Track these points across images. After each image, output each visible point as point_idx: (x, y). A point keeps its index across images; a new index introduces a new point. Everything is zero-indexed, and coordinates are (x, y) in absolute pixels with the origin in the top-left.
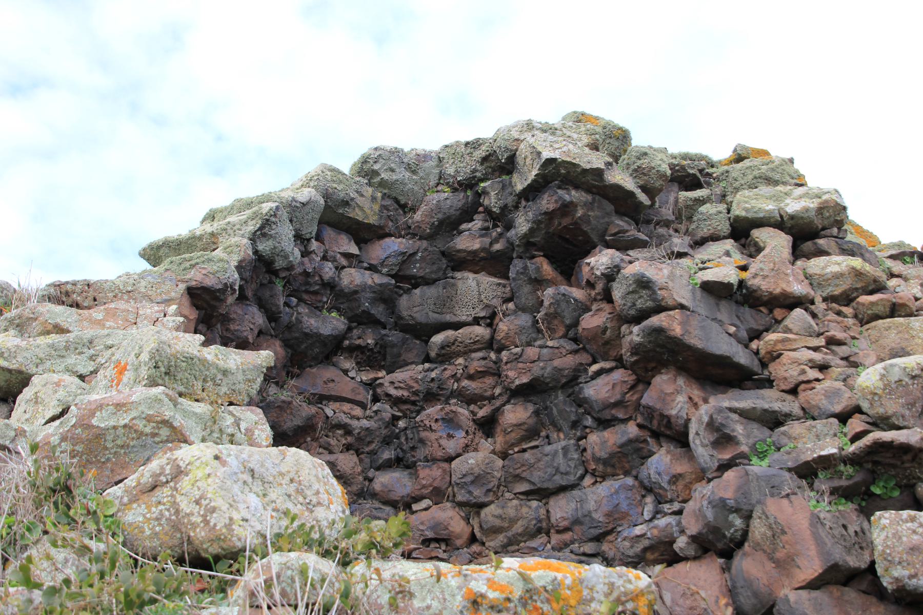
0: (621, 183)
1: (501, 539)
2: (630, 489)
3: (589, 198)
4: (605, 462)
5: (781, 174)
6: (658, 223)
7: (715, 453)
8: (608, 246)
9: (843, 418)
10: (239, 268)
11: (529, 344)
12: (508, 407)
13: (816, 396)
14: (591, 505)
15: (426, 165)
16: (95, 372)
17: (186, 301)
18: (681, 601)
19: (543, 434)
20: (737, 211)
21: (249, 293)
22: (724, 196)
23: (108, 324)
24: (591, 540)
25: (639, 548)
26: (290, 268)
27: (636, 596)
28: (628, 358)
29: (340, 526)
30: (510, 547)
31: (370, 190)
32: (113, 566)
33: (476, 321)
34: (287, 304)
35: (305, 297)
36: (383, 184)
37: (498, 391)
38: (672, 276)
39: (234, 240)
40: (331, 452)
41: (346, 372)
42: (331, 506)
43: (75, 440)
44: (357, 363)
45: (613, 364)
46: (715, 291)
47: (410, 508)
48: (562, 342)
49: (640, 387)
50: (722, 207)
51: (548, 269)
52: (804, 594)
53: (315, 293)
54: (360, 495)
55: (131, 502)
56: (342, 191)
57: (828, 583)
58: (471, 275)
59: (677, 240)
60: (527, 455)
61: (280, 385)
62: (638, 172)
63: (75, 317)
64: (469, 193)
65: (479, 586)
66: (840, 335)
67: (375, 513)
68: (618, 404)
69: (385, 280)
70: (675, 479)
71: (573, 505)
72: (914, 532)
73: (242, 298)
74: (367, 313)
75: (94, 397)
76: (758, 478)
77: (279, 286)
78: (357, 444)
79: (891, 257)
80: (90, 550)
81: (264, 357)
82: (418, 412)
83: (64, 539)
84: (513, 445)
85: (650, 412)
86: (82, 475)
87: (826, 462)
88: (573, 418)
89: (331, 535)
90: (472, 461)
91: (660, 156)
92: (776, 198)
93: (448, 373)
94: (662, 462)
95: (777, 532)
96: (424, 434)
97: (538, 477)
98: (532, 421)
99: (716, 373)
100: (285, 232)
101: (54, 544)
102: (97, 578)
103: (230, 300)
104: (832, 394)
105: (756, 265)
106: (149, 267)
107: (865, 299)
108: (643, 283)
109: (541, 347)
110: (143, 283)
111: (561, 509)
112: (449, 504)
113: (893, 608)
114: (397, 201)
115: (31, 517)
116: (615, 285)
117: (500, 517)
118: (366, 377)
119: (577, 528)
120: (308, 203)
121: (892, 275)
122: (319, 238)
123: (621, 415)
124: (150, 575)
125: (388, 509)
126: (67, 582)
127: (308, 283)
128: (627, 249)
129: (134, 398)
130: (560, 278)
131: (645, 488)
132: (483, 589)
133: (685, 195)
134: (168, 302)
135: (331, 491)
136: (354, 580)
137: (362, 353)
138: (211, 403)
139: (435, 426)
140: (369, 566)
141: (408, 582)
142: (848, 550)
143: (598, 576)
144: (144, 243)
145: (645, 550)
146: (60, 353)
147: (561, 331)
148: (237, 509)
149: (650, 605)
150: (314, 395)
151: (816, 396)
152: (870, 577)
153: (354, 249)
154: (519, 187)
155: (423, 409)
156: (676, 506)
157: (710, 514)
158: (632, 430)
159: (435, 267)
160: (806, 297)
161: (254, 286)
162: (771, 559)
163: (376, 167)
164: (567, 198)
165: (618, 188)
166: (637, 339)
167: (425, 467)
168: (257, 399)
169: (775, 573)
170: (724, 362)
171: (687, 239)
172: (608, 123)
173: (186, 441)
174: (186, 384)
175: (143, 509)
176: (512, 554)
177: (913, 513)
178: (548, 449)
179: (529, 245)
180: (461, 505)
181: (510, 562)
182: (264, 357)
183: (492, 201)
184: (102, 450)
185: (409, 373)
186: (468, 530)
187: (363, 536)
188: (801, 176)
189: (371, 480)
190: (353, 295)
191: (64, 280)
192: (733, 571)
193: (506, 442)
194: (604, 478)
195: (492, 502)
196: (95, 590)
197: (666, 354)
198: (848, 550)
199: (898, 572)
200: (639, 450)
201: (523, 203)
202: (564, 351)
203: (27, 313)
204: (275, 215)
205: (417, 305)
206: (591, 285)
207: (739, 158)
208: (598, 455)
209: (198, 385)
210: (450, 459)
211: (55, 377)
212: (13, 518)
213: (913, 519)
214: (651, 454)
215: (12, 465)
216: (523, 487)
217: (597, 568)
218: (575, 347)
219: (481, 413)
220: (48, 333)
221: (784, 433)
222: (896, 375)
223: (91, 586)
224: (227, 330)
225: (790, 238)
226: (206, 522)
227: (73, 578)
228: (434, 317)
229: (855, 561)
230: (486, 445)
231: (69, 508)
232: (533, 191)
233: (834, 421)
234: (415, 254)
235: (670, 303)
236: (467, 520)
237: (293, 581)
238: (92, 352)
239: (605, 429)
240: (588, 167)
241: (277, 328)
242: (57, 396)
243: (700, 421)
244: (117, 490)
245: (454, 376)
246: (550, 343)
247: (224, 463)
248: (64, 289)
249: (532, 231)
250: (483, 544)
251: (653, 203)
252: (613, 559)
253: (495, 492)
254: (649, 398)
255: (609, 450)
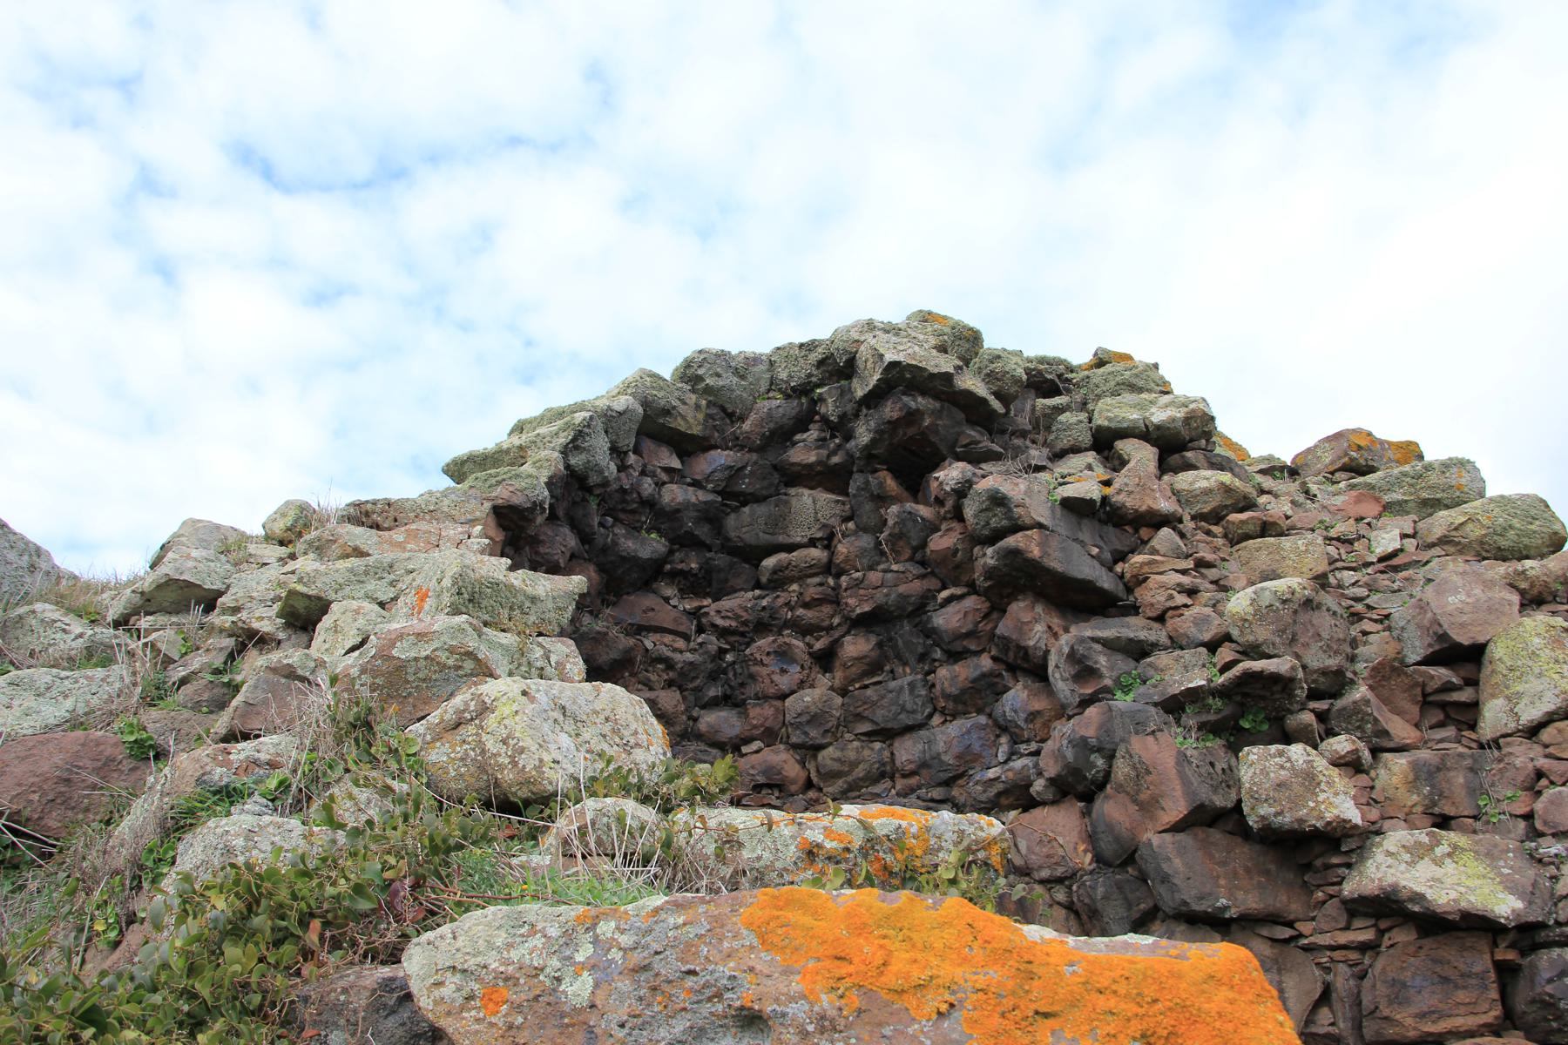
0: (972, 388)
1: (840, 784)
2: (984, 727)
3: (938, 405)
4: (956, 699)
5: (1146, 381)
6: (1013, 433)
7: (1076, 687)
8: (959, 459)
9: (1212, 646)
10: (549, 484)
11: (871, 568)
12: (848, 638)
13: (1184, 624)
14: (940, 746)
15: (755, 369)
16: (395, 599)
17: (492, 522)
18: (1037, 849)
19: (887, 668)
20: (1099, 421)
21: (561, 513)
22: (1085, 404)
23: (409, 547)
24: (940, 785)
25: (993, 791)
26: (605, 483)
27: (987, 845)
28: (981, 582)
29: (660, 769)
30: (851, 793)
31: (694, 397)
32: (417, 809)
33: (812, 543)
34: (601, 524)
35: (622, 516)
36: (708, 390)
37: (836, 621)
38: (1029, 492)
39: (544, 454)
40: (651, 689)
41: (667, 600)
42: (650, 747)
43: (375, 673)
44: (680, 590)
45: (965, 590)
46: (1075, 508)
47: (739, 750)
48: (909, 565)
49: (995, 615)
50: (1083, 416)
51: (891, 483)
52: (1168, 837)
53: (633, 512)
54: (683, 736)
55: (434, 740)
56: (662, 398)
57: (1193, 825)
58: (806, 492)
59: (1034, 452)
60: (869, 692)
61: (595, 614)
62: (990, 377)
63: (375, 539)
64: (804, 400)
65: (815, 835)
66: (1209, 556)
67: (700, 756)
68: (970, 635)
69: (711, 497)
70: (1032, 716)
71: (920, 747)
72: (1282, 767)
73: (553, 517)
74: (690, 534)
75: (395, 626)
76: (1122, 714)
77: (593, 504)
78: (680, 680)
79: (1261, 472)
80: (393, 791)
81: (576, 583)
82: (748, 645)
83: (366, 778)
84: (853, 681)
85: (1005, 643)
86: (383, 710)
87: (1194, 695)
88: (920, 650)
89: (651, 779)
90: (808, 697)
91: (1015, 359)
92: (1141, 407)
93: (781, 601)
94: (1018, 698)
95: (1142, 771)
96: (754, 669)
97: (880, 715)
98: (874, 654)
99: (1077, 600)
100: (600, 444)
101: (356, 783)
102: (400, 820)
103: (540, 520)
104: (1201, 621)
105: (1120, 480)
106: (452, 484)
107: (1235, 517)
108: (998, 500)
109: (885, 571)
110: (446, 502)
111: (907, 751)
112: (782, 747)
113: (1258, 847)
114: (723, 409)
115: (332, 754)
116: (966, 502)
117: (838, 760)
118: (689, 605)
119: (924, 772)
120: (625, 412)
121: (1263, 492)
122: (637, 451)
123: (973, 647)
124: (454, 819)
125: (714, 751)
126: (370, 823)
127: (624, 501)
128: (979, 462)
129: (435, 628)
130: (905, 494)
131: (1000, 727)
132: (820, 838)
133: (1041, 402)
134: (472, 522)
135: (651, 731)
136: (676, 828)
137: (686, 578)
138: (519, 634)
139: (766, 660)
140: (693, 814)
141: (737, 831)
142: (1215, 789)
143: (946, 824)
144: (448, 458)
145: (999, 794)
146: (358, 578)
147: (907, 553)
148: (547, 750)
149: (1004, 854)
150: (632, 625)
151: (1184, 624)
152: (1236, 817)
153: (676, 463)
154: (860, 393)
155: (753, 641)
156: (1033, 746)
157: (1070, 755)
158: (986, 662)
159: (766, 483)
160: (1173, 514)
161: (565, 504)
162: (1135, 801)
163: (700, 372)
164: (913, 405)
165: (969, 394)
166: (991, 562)
167: (755, 705)
168: (569, 630)
169: (1138, 816)
170: (1087, 586)
171: (1045, 451)
172: (958, 323)
173: (491, 675)
174: (492, 612)
175: (447, 748)
176: (852, 801)
177: (1281, 747)
178: (892, 684)
179: (871, 458)
180: (795, 747)
181: (847, 809)
182: (576, 583)
183: (830, 408)
184: (402, 684)
185: (738, 601)
186: (803, 775)
187: (686, 781)
188: (1166, 383)
189: (695, 720)
190: (674, 514)
191: (364, 499)
192: (1094, 815)
193: (845, 678)
194: (954, 716)
195: (830, 744)
196: (398, 833)
197: (1025, 579)
198: (1215, 789)
199: (1265, 810)
200: (994, 685)
201: (864, 411)
202: (910, 576)
203: (326, 535)
204: (589, 426)
205: (746, 524)
206: (939, 502)
207: (1100, 361)
208: (948, 691)
209: (505, 613)
210: (783, 697)
211: (355, 604)
212: (314, 755)
213: (1281, 754)
214: (1007, 689)
215: (312, 698)
216: (865, 727)
217: (946, 815)
218: (923, 571)
219: (818, 645)
220: (348, 556)
221: (1150, 665)
222: (1267, 599)
223: (395, 828)
224: (537, 553)
225: (1155, 450)
226: (515, 764)
227: (376, 819)
228: (765, 538)
229: (1221, 801)
230: (824, 681)
231: (370, 745)
232: (875, 398)
233: (1203, 650)
234: (744, 467)
235: (1028, 521)
236: (802, 763)
237: (610, 829)
238: (392, 577)
239: (956, 662)
240: (936, 371)
241: (591, 553)
242: (356, 624)
243: (1060, 652)
244: (419, 727)
245: (787, 604)
246: (895, 567)
247: (533, 700)
248: (364, 508)
249: (873, 441)
250: (820, 790)
251: (1008, 411)
252: (964, 805)
253: (834, 734)
254: (1004, 628)
255: (960, 685)
